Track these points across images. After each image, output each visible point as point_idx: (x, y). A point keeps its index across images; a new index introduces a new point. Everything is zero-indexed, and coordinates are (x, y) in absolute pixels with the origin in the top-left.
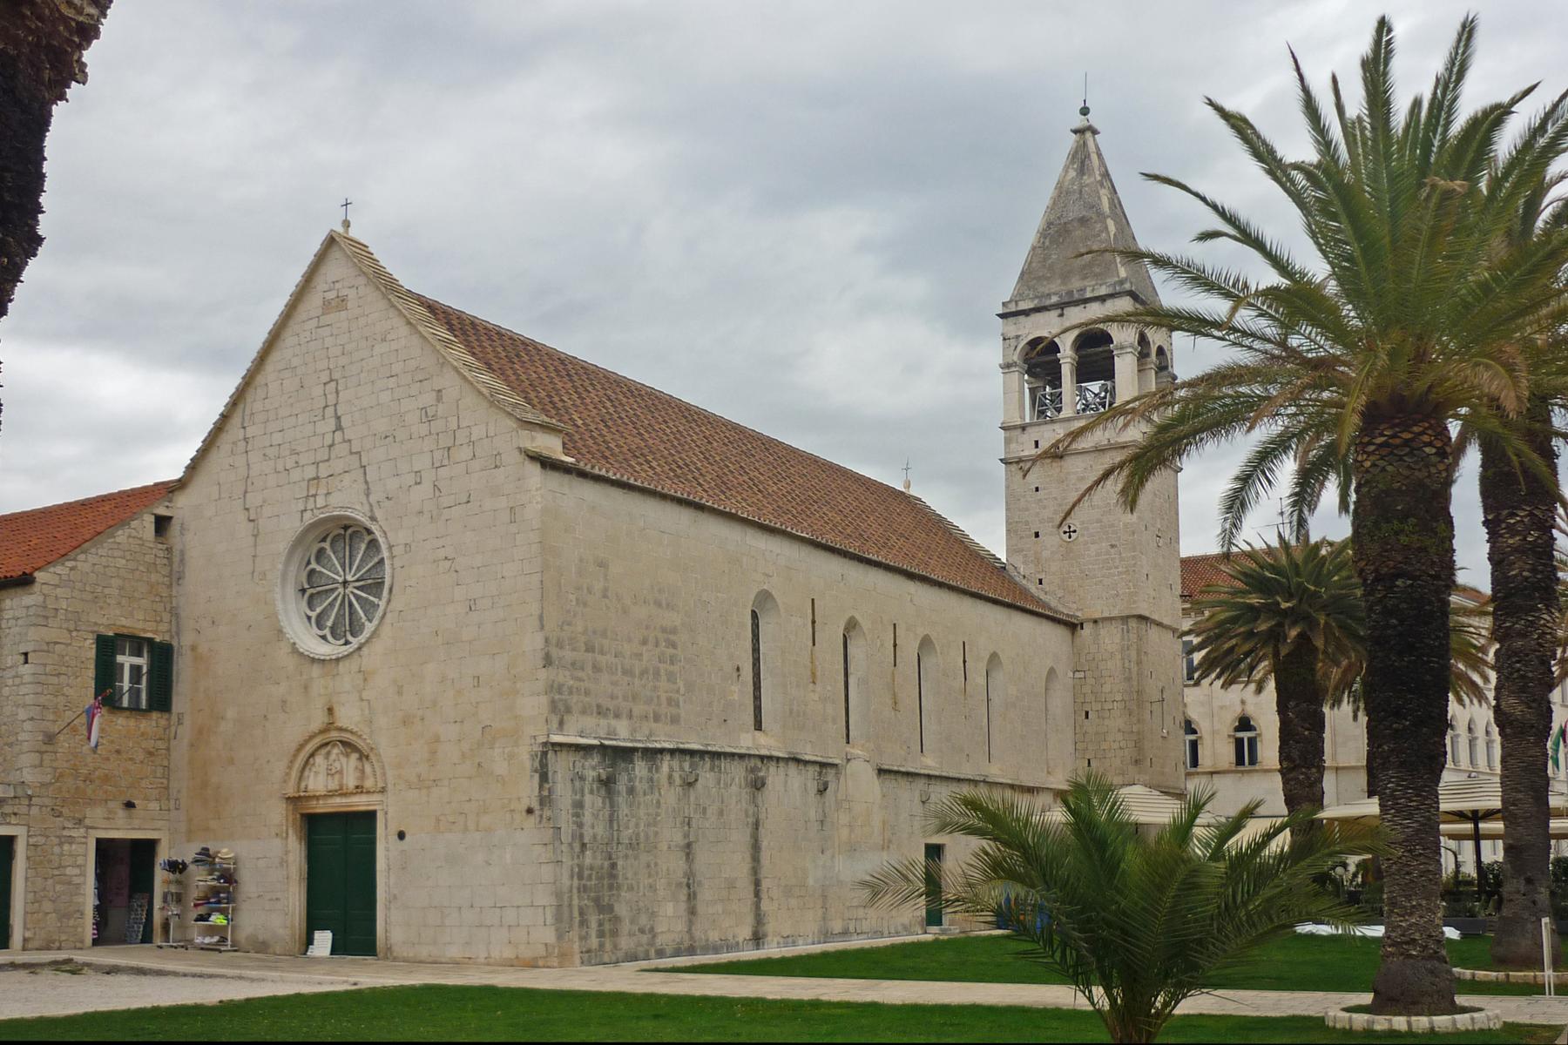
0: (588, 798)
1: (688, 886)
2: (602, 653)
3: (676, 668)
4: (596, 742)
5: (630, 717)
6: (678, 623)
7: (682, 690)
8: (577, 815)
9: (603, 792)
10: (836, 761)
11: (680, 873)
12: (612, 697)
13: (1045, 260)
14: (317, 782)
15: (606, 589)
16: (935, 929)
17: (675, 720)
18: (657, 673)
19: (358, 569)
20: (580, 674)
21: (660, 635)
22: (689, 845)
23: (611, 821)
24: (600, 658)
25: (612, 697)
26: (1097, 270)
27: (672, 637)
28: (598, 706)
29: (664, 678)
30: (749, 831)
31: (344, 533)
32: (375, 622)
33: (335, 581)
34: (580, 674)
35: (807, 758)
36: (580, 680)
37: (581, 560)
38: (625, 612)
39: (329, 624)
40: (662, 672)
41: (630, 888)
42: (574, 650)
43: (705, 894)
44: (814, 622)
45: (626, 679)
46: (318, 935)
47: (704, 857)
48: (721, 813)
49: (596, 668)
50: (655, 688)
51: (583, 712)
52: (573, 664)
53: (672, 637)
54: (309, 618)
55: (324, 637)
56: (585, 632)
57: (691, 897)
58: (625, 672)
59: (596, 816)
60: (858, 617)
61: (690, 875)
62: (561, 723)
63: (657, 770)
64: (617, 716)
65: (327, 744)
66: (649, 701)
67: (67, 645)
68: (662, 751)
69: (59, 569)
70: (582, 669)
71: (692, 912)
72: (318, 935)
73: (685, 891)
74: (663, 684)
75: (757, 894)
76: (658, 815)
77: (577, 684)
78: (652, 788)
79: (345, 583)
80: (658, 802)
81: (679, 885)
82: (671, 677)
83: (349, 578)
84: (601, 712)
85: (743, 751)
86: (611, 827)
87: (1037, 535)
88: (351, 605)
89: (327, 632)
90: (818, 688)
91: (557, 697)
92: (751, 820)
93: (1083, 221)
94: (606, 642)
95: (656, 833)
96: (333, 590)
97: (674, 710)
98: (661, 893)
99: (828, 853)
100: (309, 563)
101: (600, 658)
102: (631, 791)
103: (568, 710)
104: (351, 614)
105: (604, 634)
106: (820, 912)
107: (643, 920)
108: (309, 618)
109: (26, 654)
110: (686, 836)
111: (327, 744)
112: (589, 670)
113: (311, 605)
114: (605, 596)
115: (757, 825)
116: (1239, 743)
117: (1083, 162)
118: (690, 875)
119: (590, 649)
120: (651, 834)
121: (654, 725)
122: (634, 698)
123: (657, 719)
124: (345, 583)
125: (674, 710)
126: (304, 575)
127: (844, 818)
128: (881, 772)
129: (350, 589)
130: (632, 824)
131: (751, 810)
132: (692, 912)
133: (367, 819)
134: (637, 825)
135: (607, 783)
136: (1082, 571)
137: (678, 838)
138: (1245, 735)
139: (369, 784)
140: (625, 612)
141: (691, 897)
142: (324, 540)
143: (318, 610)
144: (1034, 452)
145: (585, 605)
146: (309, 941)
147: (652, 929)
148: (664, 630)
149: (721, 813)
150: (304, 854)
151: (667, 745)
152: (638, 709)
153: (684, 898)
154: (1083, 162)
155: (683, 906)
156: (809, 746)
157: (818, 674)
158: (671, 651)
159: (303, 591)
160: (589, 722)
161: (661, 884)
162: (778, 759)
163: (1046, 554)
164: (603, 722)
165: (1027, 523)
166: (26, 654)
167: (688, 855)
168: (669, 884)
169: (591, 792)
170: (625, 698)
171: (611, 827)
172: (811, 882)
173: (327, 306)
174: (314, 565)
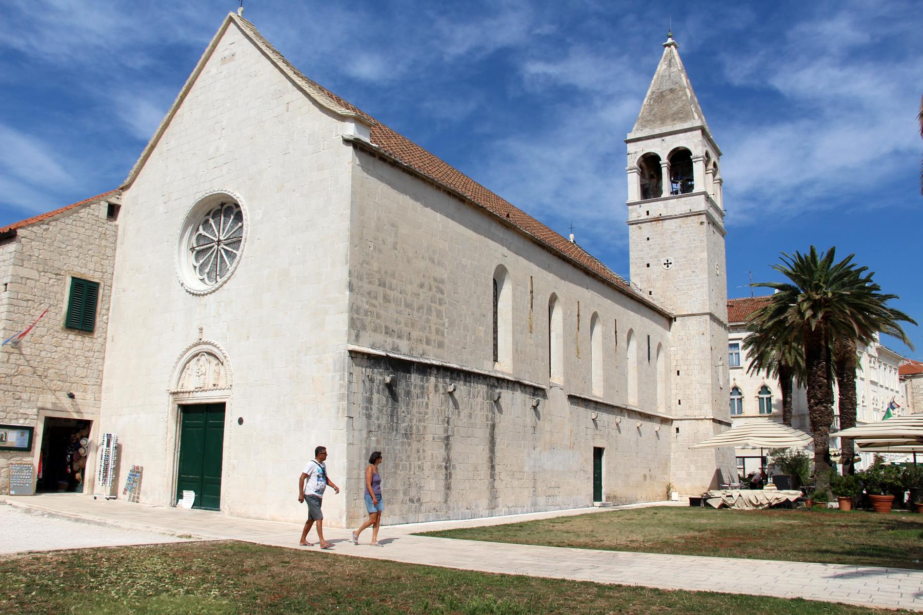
0: (376, 396)
1: (446, 468)
2: (391, 288)
3: (443, 308)
4: (384, 354)
5: (409, 339)
6: (445, 276)
7: (447, 324)
8: (367, 409)
9: (387, 393)
10: (544, 387)
11: (440, 459)
12: (397, 322)
13: (651, 111)
14: (190, 383)
15: (396, 243)
16: (597, 504)
17: (441, 345)
18: (429, 309)
19: (228, 232)
20: (374, 302)
21: (433, 283)
22: (447, 438)
23: (392, 416)
24: (389, 292)
25: (397, 322)
26: (681, 116)
27: (441, 285)
28: (386, 327)
29: (434, 314)
30: (488, 430)
31: (224, 209)
32: (234, 265)
33: (213, 241)
34: (374, 302)
35: (527, 382)
36: (374, 306)
37: (379, 219)
38: (409, 261)
39: (207, 270)
40: (433, 309)
41: (404, 468)
42: (370, 283)
43: (458, 474)
44: (532, 292)
45: (408, 310)
46: (185, 493)
47: (457, 447)
48: (470, 416)
49: (386, 299)
50: (428, 321)
51: (375, 331)
52: (369, 293)
53: (441, 285)
54: (195, 267)
55: (202, 280)
56: (379, 271)
57: (448, 476)
58: (407, 305)
59: (381, 411)
60: (558, 294)
61: (448, 460)
62: (357, 336)
63: (427, 381)
64: (400, 337)
65: (197, 355)
66: (423, 329)
67: (36, 281)
68: (431, 366)
69: (35, 229)
70: (376, 298)
71: (448, 487)
72: (185, 493)
73: (444, 471)
74: (433, 318)
75: (492, 476)
76: (426, 413)
77: (372, 309)
78: (422, 393)
79: (219, 241)
80: (427, 404)
81: (440, 467)
82: (439, 315)
83: (222, 238)
84: (388, 332)
85: (486, 373)
86: (392, 420)
87: (648, 266)
88: (222, 256)
89: (205, 276)
90: (533, 335)
91: (355, 316)
92: (490, 422)
93: (672, 91)
94: (394, 282)
95: (425, 427)
96: (211, 247)
97: (440, 338)
98: (427, 472)
99: (538, 450)
100: (198, 230)
101: (389, 292)
102: (408, 393)
103: (364, 327)
104: (221, 263)
105: (393, 276)
106: (532, 490)
107: (413, 493)
108: (195, 267)
109: (6, 285)
110: (446, 430)
111: (197, 355)
112: (381, 300)
113: (197, 259)
114: (395, 248)
115: (493, 427)
116: (761, 399)
117: (670, 61)
118: (448, 460)
119: (382, 284)
120: (421, 428)
121: (425, 347)
122: (413, 325)
123: (428, 342)
124: (219, 241)
125: (440, 338)
126: (194, 238)
127: (548, 427)
128: (571, 397)
129: (222, 245)
130: (407, 419)
131: (490, 414)
132: (448, 487)
133: (219, 409)
134: (411, 420)
135: (391, 388)
136: (675, 287)
137: (441, 433)
138: (736, 397)
139: (221, 384)
140: (409, 261)
141: (448, 476)
142: (208, 214)
143: (201, 262)
144: (646, 217)
145: (380, 251)
146: (180, 496)
147: (419, 500)
148: (435, 280)
149: (470, 416)
150: (179, 433)
151: (434, 362)
152: (415, 334)
153: (444, 477)
154: (670, 61)
155: (442, 483)
156: (527, 375)
157: (534, 326)
158: (439, 295)
159: (193, 249)
160: (380, 338)
161: (427, 465)
162: (508, 381)
163: (653, 276)
164: (389, 340)
165: (642, 259)
166: (6, 285)
167: (447, 445)
168: (433, 467)
169: (378, 392)
170: (406, 325)
171: (392, 420)
172: (526, 469)
173: (224, 60)
174: (201, 231)
